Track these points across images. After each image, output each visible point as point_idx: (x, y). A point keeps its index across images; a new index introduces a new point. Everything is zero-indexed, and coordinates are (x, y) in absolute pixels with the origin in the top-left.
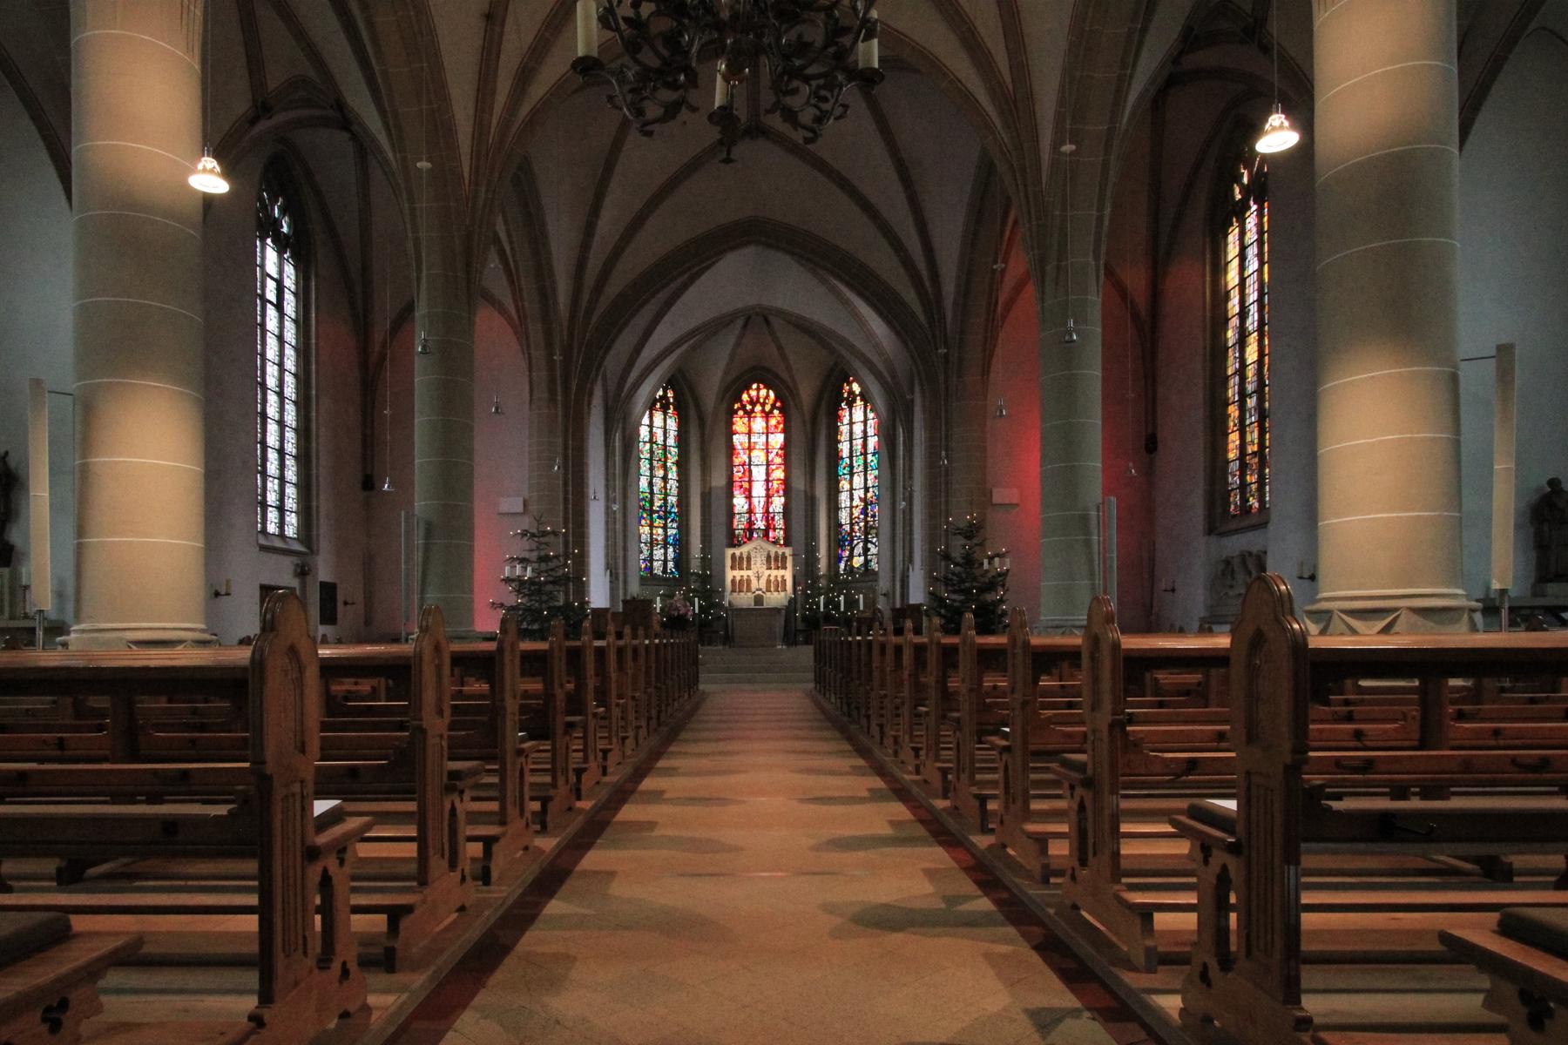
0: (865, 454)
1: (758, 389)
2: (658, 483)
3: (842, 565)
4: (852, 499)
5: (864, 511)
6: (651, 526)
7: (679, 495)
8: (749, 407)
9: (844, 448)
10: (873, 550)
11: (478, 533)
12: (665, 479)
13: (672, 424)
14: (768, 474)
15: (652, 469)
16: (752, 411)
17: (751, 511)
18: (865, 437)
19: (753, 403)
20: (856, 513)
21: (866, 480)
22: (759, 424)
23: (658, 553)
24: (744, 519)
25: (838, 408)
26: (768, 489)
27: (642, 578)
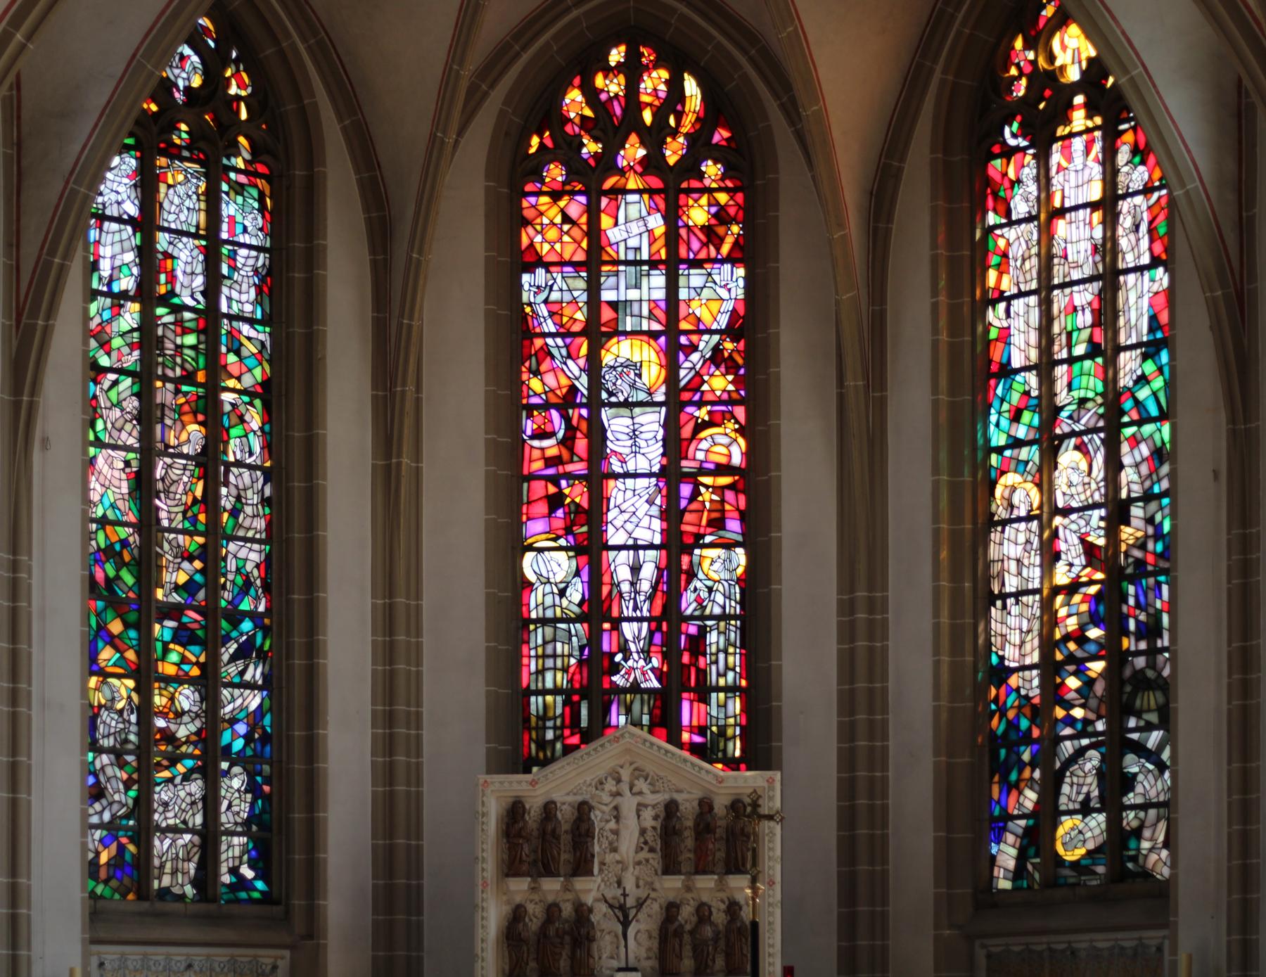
0: (1105, 350)
1: (633, 71)
2: (179, 483)
3: (1006, 854)
4: (1051, 555)
5: (1107, 608)
7: (274, 535)
8: (591, 147)
9: (1017, 331)
10: (1149, 786)
11: (834, 842)
12: (210, 463)
13: (243, 217)
14: (674, 445)
15: (147, 416)
16: (606, 162)
17: (598, 609)
18: (1109, 277)
19: (612, 124)
20: (1069, 617)
21: (1114, 465)
22: (633, 225)
23: (177, 798)
26: (671, 514)
27: (96, 912)
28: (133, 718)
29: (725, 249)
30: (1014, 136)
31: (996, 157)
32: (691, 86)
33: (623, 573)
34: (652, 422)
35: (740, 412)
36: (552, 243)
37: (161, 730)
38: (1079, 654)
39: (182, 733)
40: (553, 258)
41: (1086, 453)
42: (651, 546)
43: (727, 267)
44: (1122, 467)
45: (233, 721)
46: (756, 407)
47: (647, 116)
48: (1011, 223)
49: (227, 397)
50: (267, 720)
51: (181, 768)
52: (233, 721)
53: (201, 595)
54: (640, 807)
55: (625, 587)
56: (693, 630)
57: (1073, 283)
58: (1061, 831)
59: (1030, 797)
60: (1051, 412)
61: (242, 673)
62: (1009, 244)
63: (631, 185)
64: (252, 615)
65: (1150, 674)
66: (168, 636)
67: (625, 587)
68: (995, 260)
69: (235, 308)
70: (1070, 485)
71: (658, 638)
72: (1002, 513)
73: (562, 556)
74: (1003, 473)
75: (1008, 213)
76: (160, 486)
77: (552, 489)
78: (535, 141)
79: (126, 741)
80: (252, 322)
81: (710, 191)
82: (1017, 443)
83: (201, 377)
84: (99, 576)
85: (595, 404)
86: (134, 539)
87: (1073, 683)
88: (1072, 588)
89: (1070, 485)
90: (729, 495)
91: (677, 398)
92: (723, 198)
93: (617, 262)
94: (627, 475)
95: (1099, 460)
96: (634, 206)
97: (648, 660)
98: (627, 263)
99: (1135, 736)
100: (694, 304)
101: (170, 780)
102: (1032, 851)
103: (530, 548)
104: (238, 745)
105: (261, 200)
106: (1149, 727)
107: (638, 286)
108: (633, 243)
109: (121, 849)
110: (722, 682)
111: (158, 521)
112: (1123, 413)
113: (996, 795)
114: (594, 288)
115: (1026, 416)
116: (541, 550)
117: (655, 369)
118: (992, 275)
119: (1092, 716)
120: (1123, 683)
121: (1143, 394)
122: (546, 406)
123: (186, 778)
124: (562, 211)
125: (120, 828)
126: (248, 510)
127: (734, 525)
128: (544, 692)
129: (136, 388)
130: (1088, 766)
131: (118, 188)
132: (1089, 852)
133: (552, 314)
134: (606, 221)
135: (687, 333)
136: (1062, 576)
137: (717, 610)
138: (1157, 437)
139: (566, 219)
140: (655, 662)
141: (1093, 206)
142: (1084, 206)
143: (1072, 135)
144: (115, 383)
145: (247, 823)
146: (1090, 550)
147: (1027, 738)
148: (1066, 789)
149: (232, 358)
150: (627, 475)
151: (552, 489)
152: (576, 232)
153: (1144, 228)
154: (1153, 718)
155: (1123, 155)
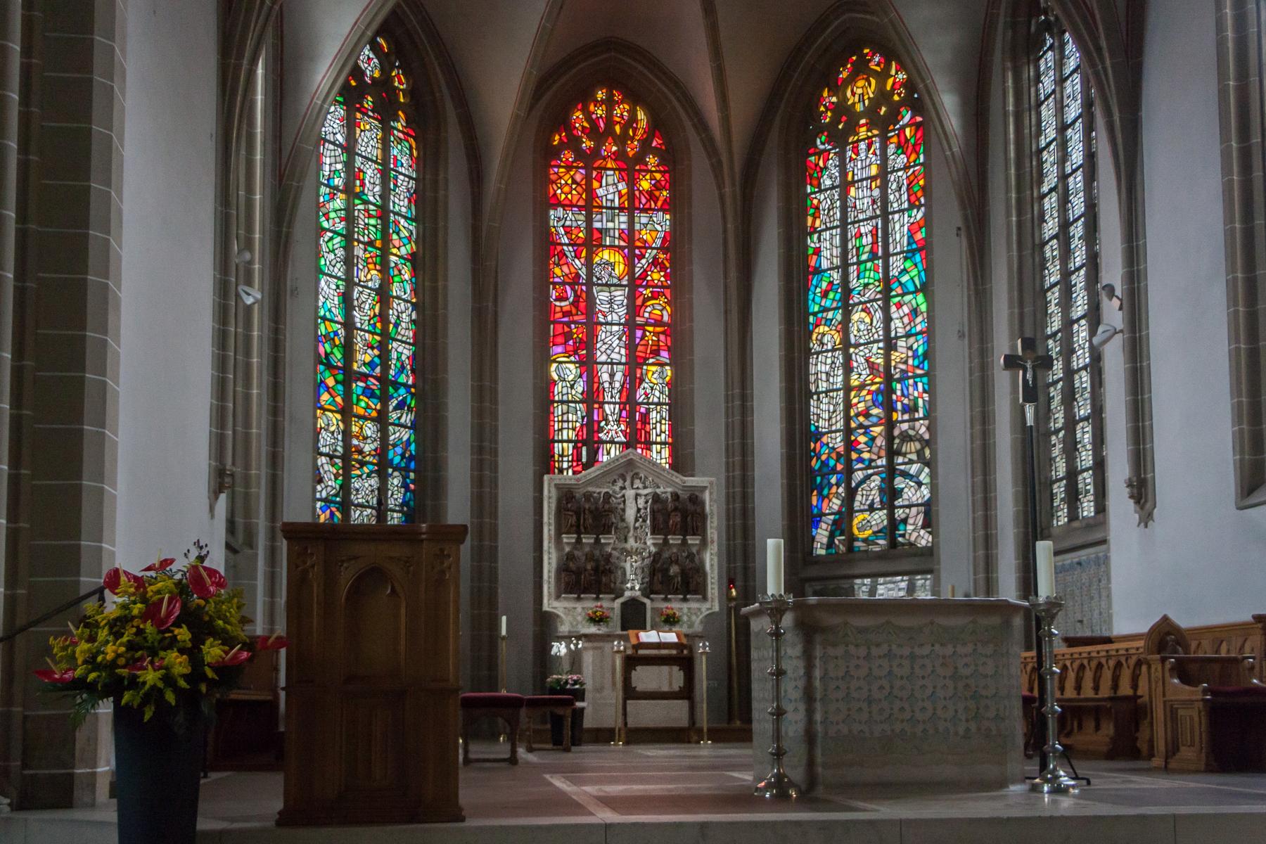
0: (882, 253)
1: (610, 103)
6: (346, 412)
8: (587, 144)
10: (914, 494)
12: (383, 295)
13: (402, 154)
14: (634, 309)
15: (349, 261)
16: (595, 153)
22: (610, 188)
23: (364, 486)
24: (576, 417)
25: (807, 146)
26: (631, 347)
28: (340, 437)
29: (659, 203)
30: (823, 144)
31: (811, 155)
32: (641, 115)
33: (605, 377)
34: (620, 295)
35: (667, 292)
36: (566, 194)
37: (356, 446)
38: (866, 423)
39: (367, 449)
40: (567, 202)
41: (869, 313)
42: (620, 363)
43: (661, 214)
44: (891, 319)
45: (395, 446)
46: (678, 290)
47: (618, 128)
48: (821, 191)
49: (393, 258)
50: (413, 447)
51: (366, 469)
52: (395, 446)
53: (378, 370)
54: (637, 495)
55: (606, 385)
56: (643, 410)
57: (859, 221)
58: (855, 521)
59: (836, 504)
60: (847, 292)
61: (399, 418)
62: (820, 202)
63: (609, 165)
64: (405, 385)
65: (911, 433)
66: (359, 392)
67: (606, 385)
68: (812, 211)
69: (397, 208)
70: (859, 331)
71: (624, 413)
72: (817, 348)
73: (572, 366)
74: (817, 325)
75: (819, 185)
76: (356, 303)
77: (566, 329)
78: (557, 137)
79: (336, 450)
80: (405, 218)
81: (652, 172)
82: (826, 310)
83: (378, 244)
84: (321, 350)
85: (590, 284)
86: (342, 332)
87: (862, 439)
88: (862, 387)
89: (859, 331)
90: (662, 337)
91: (635, 283)
92: (658, 176)
93: (602, 207)
94: (607, 324)
95: (879, 315)
96: (611, 177)
97: (619, 425)
98: (607, 208)
99: (902, 467)
100: (643, 232)
101: (360, 476)
102: (838, 533)
103: (555, 361)
104: (397, 460)
105: (411, 149)
106: (911, 462)
107: (613, 221)
108: (610, 197)
109: (332, 514)
110: (659, 439)
111: (354, 323)
112: (892, 290)
113: (814, 503)
114: (589, 221)
115: (831, 295)
116: (560, 363)
117: (622, 266)
118: (810, 220)
119: (874, 457)
120: (894, 438)
121: (904, 279)
122: (563, 283)
123: (369, 476)
124: (572, 177)
125: (332, 502)
126: (404, 325)
127: (665, 354)
128: (562, 441)
129: (343, 244)
130: (873, 485)
131: (333, 126)
132: (874, 533)
133: (567, 233)
134: (596, 184)
135: (639, 248)
136: (855, 381)
137: (656, 400)
138: (914, 302)
139: (574, 182)
140: (623, 427)
141: (873, 178)
142: (866, 179)
143: (859, 141)
144: (331, 239)
145: (402, 505)
146: (872, 366)
147: (834, 471)
148: (858, 498)
149: (395, 237)
150: (607, 324)
151: (566, 329)
152: (579, 189)
153: (904, 188)
154: (914, 457)
155: (891, 149)
